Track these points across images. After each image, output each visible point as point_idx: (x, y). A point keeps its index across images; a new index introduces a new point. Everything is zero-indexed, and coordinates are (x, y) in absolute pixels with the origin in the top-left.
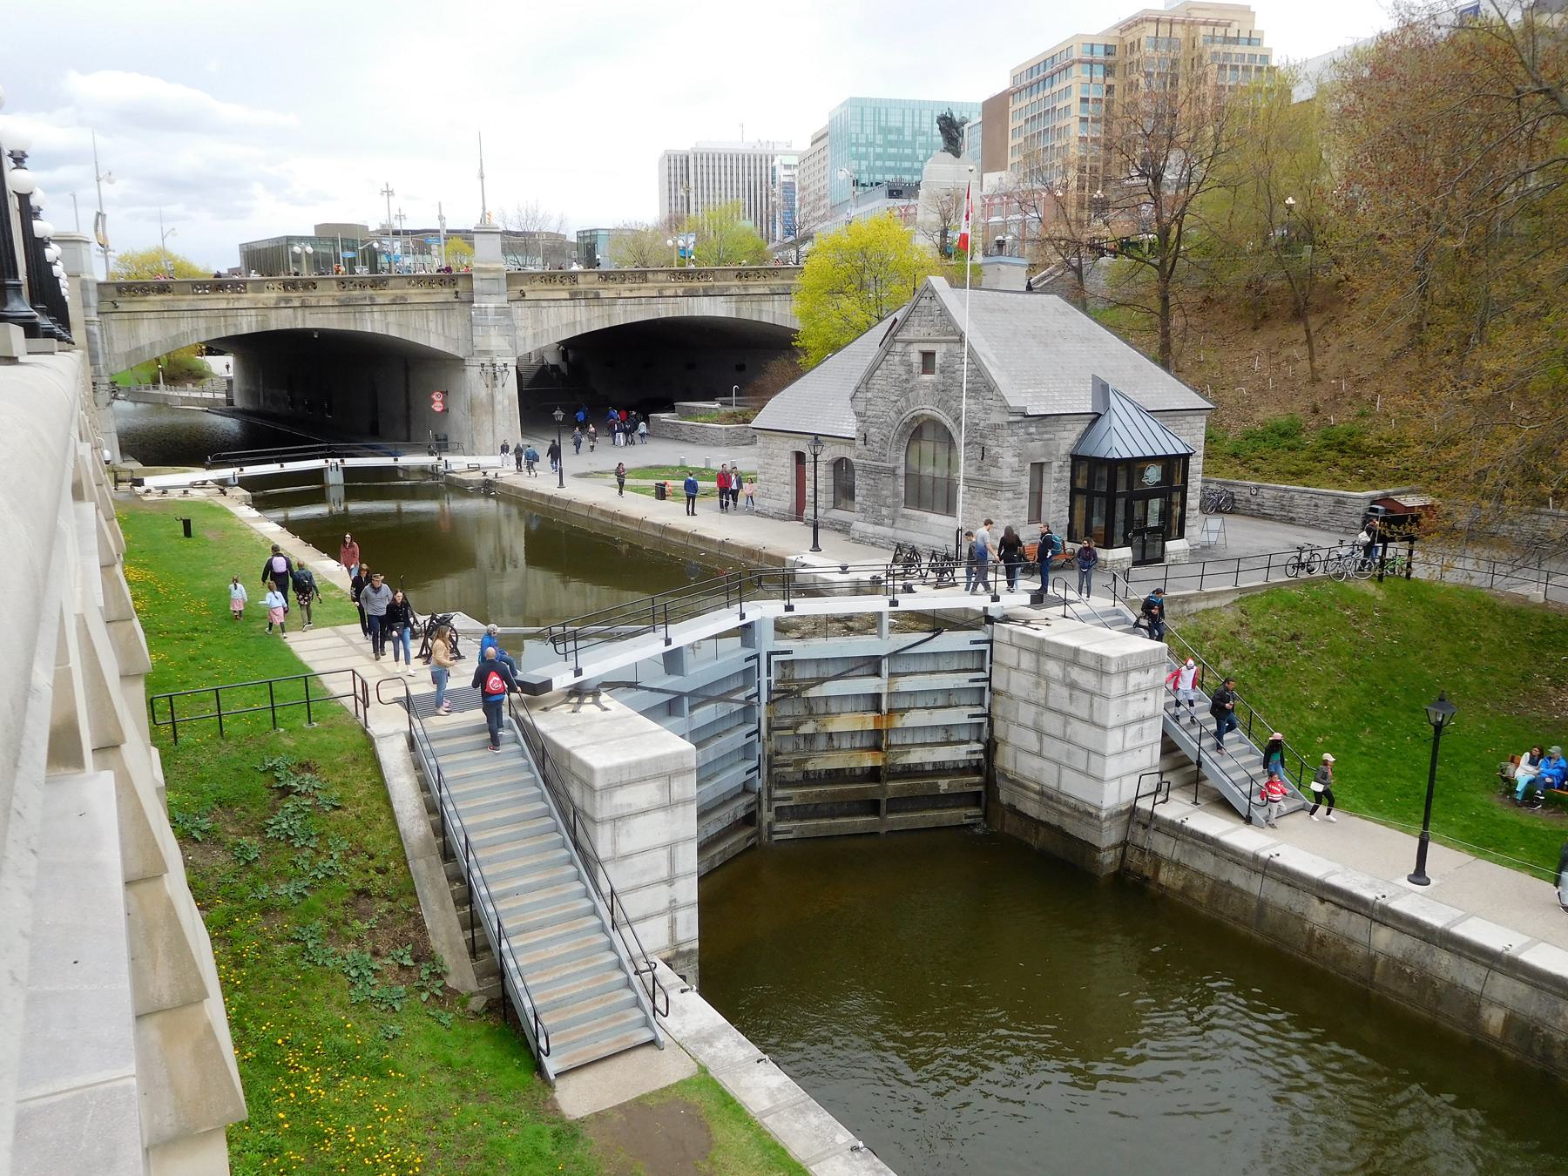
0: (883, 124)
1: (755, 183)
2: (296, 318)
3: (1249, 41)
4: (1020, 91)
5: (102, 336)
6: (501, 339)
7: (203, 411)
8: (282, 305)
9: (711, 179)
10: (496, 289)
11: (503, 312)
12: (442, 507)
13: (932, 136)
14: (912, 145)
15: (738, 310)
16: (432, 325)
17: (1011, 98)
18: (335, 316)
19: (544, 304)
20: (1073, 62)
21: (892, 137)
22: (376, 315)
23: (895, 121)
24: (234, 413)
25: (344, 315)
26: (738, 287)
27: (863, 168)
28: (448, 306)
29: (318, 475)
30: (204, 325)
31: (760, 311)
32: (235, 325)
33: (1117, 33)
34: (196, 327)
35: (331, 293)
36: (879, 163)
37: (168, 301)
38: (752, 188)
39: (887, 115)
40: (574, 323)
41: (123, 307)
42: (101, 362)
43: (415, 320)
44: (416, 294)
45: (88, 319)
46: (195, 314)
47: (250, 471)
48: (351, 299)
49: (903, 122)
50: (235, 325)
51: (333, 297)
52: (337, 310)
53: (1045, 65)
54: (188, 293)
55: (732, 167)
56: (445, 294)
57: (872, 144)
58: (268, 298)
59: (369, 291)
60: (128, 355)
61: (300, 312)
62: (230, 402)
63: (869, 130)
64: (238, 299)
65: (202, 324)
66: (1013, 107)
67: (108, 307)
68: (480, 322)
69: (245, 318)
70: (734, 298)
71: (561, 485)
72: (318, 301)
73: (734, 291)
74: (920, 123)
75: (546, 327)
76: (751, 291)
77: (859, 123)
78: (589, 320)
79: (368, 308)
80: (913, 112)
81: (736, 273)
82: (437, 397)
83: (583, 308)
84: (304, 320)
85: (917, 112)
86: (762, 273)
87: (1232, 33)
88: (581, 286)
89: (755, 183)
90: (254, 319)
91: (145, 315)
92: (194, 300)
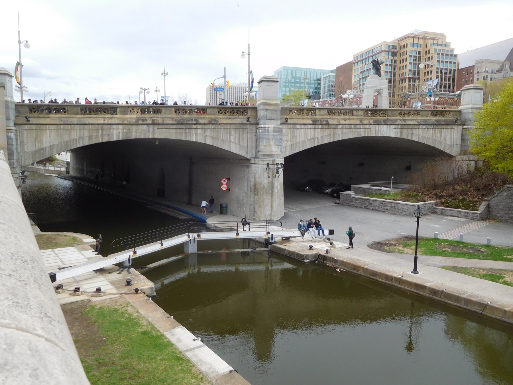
0: (294, 76)
1: (240, 96)
2: (148, 131)
4: (357, 62)
5: (17, 140)
6: (276, 147)
7: (56, 176)
8: (140, 122)
9: (233, 93)
10: (274, 117)
11: (278, 131)
12: (267, 268)
13: (311, 80)
15: (401, 133)
16: (232, 138)
17: (353, 65)
18: (173, 131)
19: (298, 126)
20: (382, 51)
21: (297, 80)
22: (199, 131)
24: (71, 178)
26: (400, 120)
28: (243, 126)
29: (180, 249)
30: (88, 135)
31: (412, 134)
32: (109, 135)
33: (397, 42)
34: (82, 135)
35: (171, 116)
36: (292, 89)
37: (64, 117)
38: (237, 98)
39: (295, 73)
40: (314, 139)
41: (33, 121)
42: (15, 157)
43: (222, 134)
44: (223, 118)
45: (9, 128)
46: (82, 127)
47: (143, 251)
48: (183, 120)
49: (301, 75)
50: (109, 135)
51: (172, 119)
52: (175, 127)
53: (363, 55)
54: (78, 113)
55: (232, 91)
56: (240, 119)
57: (290, 82)
58: (130, 118)
59: (194, 116)
60: (34, 153)
61: (151, 128)
62: (68, 173)
63: (289, 78)
64: (111, 118)
65: (86, 133)
66: (355, 67)
67: (22, 121)
68: (264, 136)
69: (115, 131)
70: (399, 126)
71: (415, 271)
72: (163, 121)
73: (399, 122)
74: (307, 76)
75: (298, 140)
76: (408, 123)
77: (286, 75)
78: (322, 137)
79: (194, 126)
80: (304, 72)
81: (399, 112)
82: (224, 182)
83: (319, 130)
84: (153, 133)
85: (306, 72)
86: (412, 113)
87: (440, 43)
88: (318, 117)
89: (240, 96)
90: (121, 131)
91: (48, 127)
92: (82, 118)
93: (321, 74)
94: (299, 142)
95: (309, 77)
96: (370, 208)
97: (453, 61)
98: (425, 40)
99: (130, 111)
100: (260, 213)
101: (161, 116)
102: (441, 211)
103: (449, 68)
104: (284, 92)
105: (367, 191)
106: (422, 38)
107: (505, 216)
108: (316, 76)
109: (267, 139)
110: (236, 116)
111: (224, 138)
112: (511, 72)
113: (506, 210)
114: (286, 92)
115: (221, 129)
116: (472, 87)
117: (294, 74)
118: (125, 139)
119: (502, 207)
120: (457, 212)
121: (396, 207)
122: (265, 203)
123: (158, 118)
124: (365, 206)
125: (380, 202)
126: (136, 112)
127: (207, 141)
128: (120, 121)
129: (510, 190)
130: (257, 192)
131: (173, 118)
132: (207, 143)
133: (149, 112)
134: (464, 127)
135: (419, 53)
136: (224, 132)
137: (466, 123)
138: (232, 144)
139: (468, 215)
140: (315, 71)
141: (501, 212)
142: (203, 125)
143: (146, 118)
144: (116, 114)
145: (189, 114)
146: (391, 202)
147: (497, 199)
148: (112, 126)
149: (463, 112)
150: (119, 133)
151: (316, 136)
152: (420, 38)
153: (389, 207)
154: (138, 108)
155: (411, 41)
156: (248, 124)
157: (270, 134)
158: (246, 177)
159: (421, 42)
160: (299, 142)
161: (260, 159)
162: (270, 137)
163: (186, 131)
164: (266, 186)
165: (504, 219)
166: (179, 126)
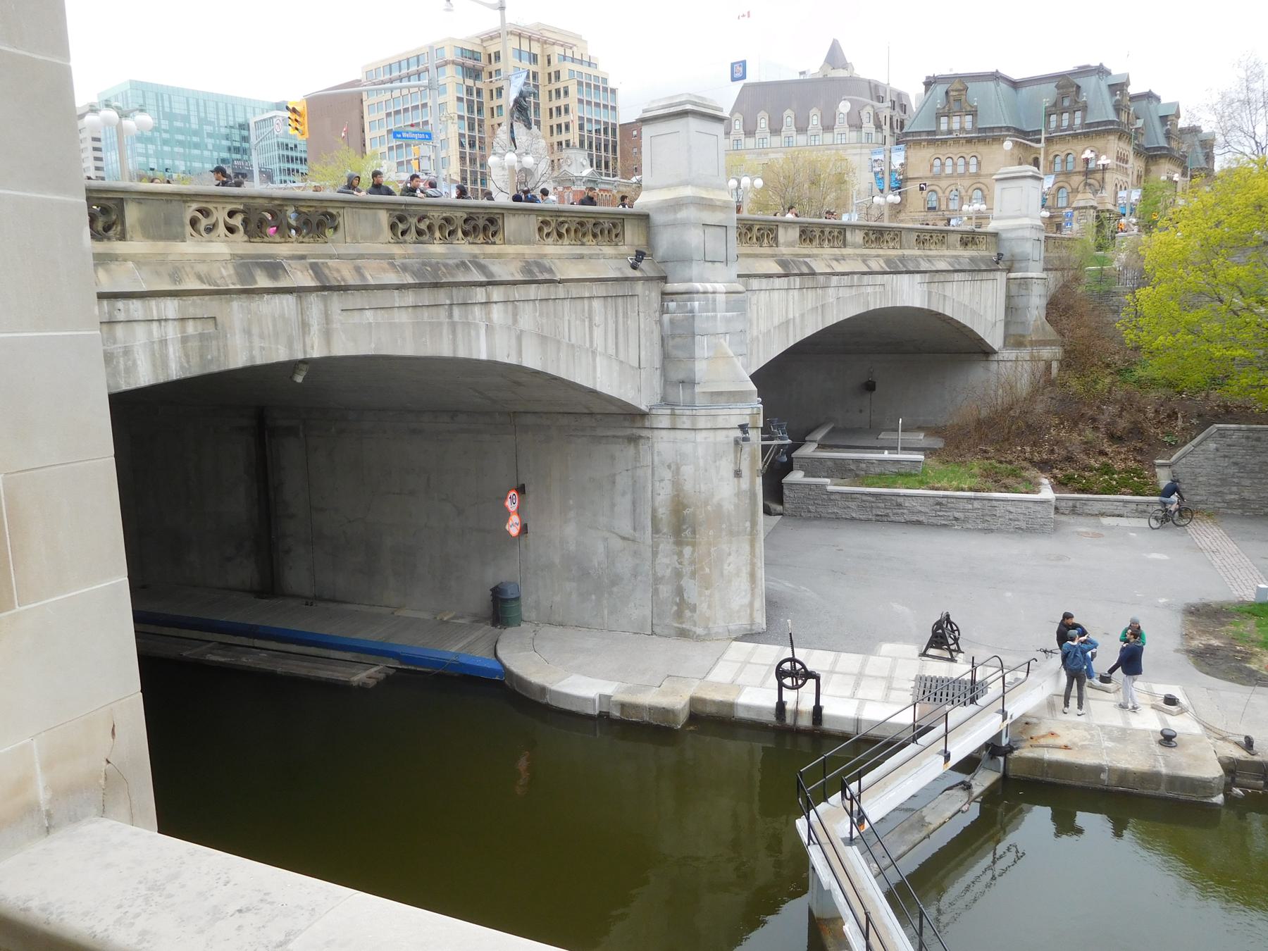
0: (167, 110)
3: (590, 64)
8: (263, 282)
13: (219, 127)
14: (195, 133)
18: (403, 317)
20: (446, 63)
21: (178, 124)
22: (497, 313)
23: (179, 108)
25: (426, 315)
27: (151, 152)
33: (478, 41)
36: (166, 148)
40: (787, 322)
52: (410, 298)
53: (400, 66)
69: (140, 331)
79: (480, 294)
84: (327, 334)
93: (249, 110)
94: (758, 337)
95: (212, 117)
96: (897, 519)
97: (610, 104)
98: (545, 46)
99: (194, 222)
100: (709, 607)
101: (342, 249)
102: (1071, 503)
103: (603, 119)
104: (140, 155)
105: (852, 467)
106: (538, 40)
107: (1212, 499)
108: (234, 117)
109: (712, 335)
110: (590, 248)
111: (573, 341)
112: (747, 139)
113: (1217, 486)
114: (147, 156)
115: (565, 301)
116: (1031, 174)
117: (167, 104)
118: (195, 371)
119: (1204, 479)
120: (1118, 504)
121: (987, 512)
122: (728, 569)
123: (331, 257)
124: (877, 515)
125: (932, 501)
126: (222, 229)
127: (524, 356)
128: (158, 273)
129: (1224, 437)
130: (694, 532)
131: (392, 257)
132: (525, 364)
133: (282, 229)
134: (1012, 275)
135: (535, 75)
136: (574, 316)
137: (1017, 265)
138: (598, 359)
139: (1150, 509)
140: (230, 103)
141: (1203, 492)
142: (511, 289)
143: (278, 255)
144: (122, 237)
145: (444, 240)
146: (970, 499)
147: (1192, 459)
148: (120, 304)
149: (1004, 235)
150: (163, 342)
151: (791, 316)
152: (533, 40)
153: (964, 510)
154: (230, 207)
155: (513, 43)
156: (639, 279)
157: (719, 315)
158: (623, 481)
159: (536, 49)
160: (758, 337)
161: (703, 412)
162: (721, 328)
163: (451, 316)
164: (728, 507)
165: (1211, 507)
166: (426, 297)
